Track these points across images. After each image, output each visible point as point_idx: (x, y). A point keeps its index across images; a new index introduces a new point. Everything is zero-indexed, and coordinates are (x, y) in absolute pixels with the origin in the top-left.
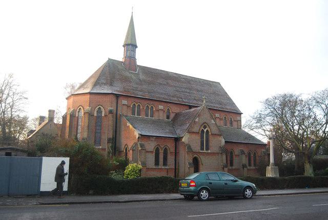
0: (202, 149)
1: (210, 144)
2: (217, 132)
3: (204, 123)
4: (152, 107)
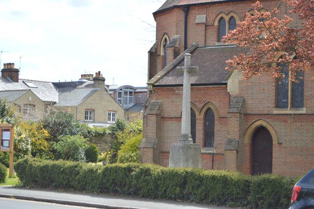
3: (115, 111)
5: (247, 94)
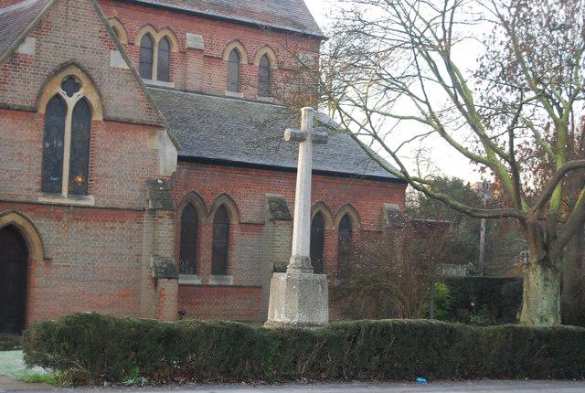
0: (50, 186)
1: (98, 168)
2: (140, 114)
3: (64, 67)
4: (166, 38)
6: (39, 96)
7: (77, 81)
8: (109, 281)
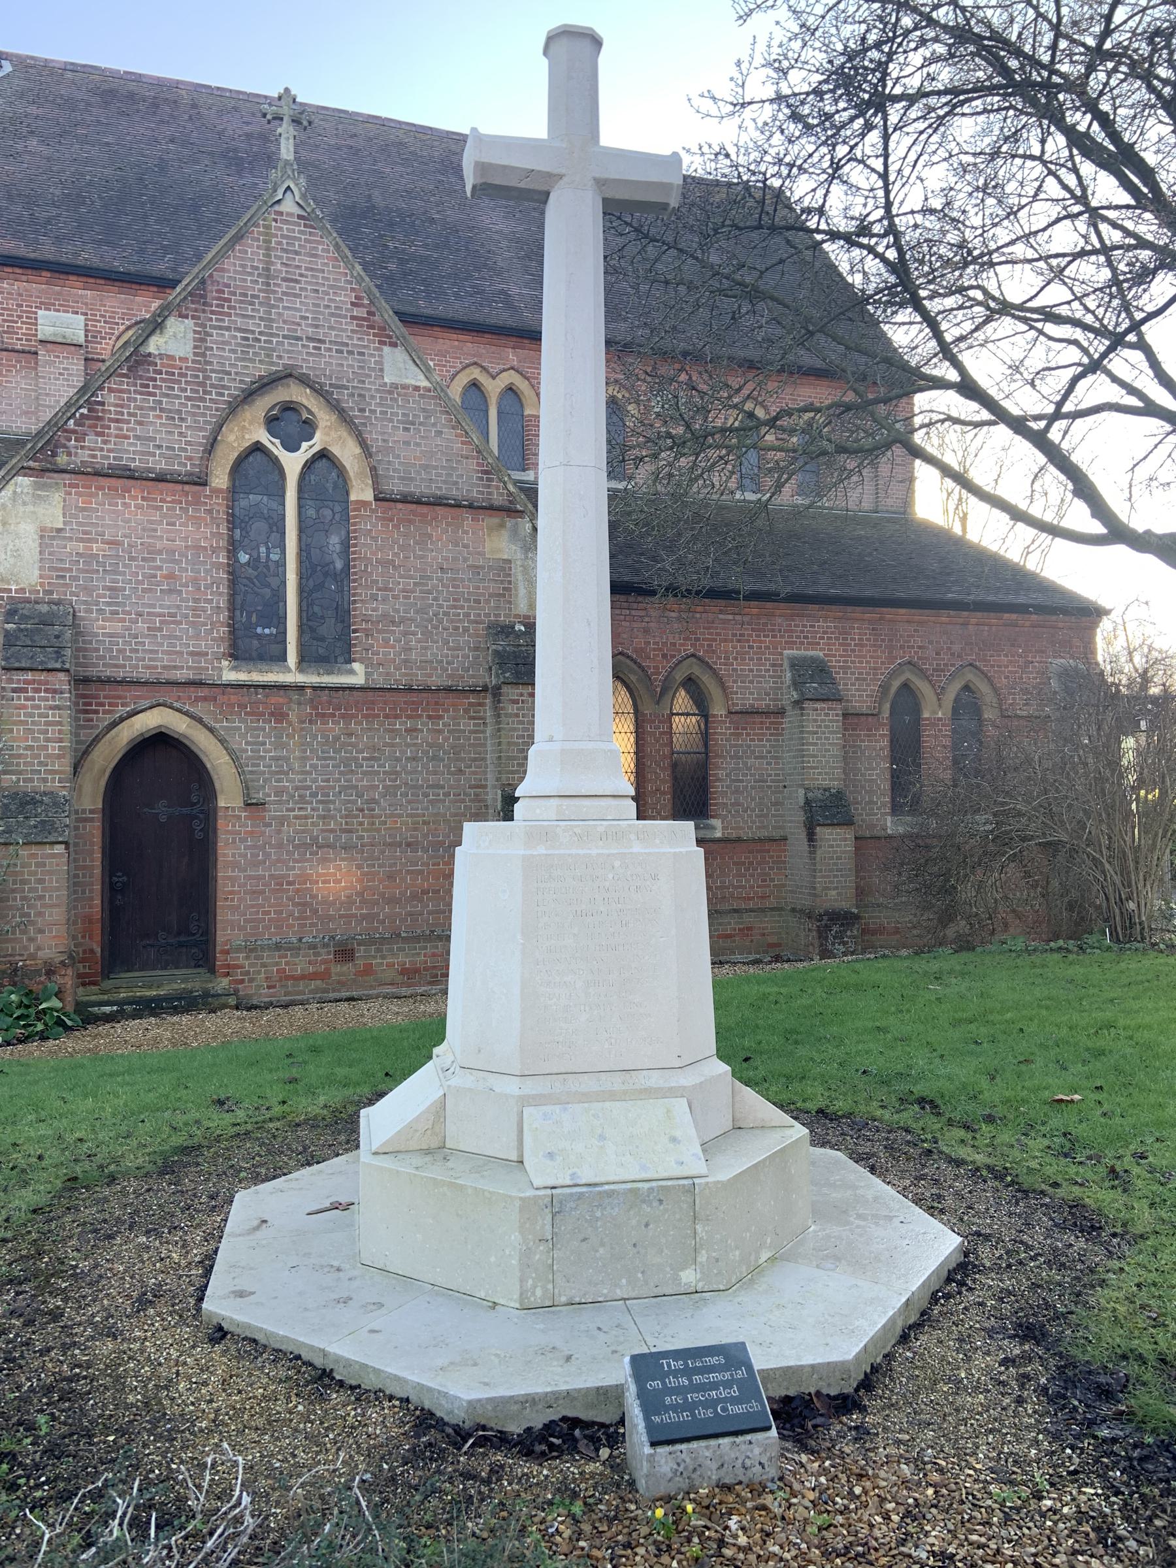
5: (88, 590)
6: (212, 445)
7: (305, 415)
8: (409, 845)
